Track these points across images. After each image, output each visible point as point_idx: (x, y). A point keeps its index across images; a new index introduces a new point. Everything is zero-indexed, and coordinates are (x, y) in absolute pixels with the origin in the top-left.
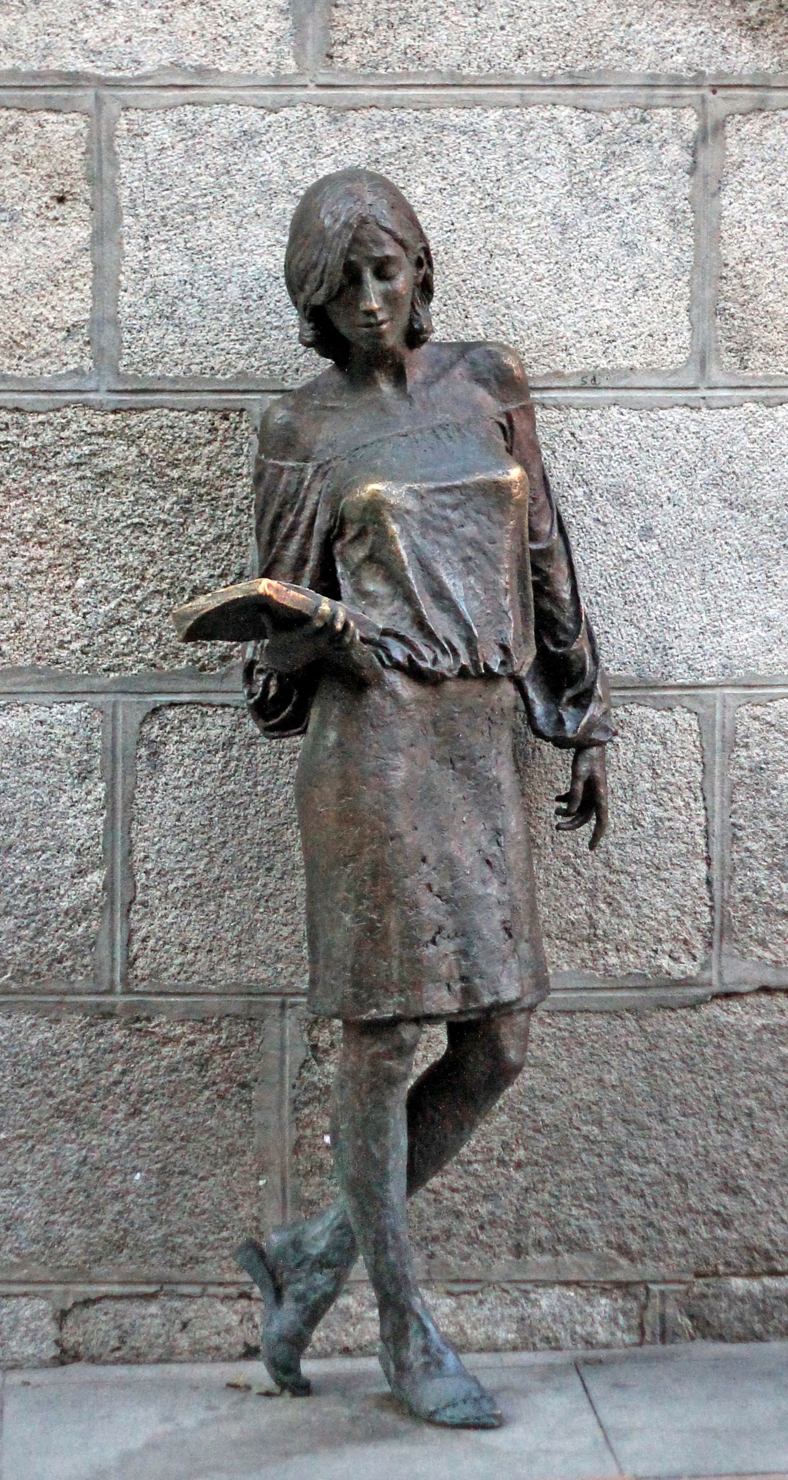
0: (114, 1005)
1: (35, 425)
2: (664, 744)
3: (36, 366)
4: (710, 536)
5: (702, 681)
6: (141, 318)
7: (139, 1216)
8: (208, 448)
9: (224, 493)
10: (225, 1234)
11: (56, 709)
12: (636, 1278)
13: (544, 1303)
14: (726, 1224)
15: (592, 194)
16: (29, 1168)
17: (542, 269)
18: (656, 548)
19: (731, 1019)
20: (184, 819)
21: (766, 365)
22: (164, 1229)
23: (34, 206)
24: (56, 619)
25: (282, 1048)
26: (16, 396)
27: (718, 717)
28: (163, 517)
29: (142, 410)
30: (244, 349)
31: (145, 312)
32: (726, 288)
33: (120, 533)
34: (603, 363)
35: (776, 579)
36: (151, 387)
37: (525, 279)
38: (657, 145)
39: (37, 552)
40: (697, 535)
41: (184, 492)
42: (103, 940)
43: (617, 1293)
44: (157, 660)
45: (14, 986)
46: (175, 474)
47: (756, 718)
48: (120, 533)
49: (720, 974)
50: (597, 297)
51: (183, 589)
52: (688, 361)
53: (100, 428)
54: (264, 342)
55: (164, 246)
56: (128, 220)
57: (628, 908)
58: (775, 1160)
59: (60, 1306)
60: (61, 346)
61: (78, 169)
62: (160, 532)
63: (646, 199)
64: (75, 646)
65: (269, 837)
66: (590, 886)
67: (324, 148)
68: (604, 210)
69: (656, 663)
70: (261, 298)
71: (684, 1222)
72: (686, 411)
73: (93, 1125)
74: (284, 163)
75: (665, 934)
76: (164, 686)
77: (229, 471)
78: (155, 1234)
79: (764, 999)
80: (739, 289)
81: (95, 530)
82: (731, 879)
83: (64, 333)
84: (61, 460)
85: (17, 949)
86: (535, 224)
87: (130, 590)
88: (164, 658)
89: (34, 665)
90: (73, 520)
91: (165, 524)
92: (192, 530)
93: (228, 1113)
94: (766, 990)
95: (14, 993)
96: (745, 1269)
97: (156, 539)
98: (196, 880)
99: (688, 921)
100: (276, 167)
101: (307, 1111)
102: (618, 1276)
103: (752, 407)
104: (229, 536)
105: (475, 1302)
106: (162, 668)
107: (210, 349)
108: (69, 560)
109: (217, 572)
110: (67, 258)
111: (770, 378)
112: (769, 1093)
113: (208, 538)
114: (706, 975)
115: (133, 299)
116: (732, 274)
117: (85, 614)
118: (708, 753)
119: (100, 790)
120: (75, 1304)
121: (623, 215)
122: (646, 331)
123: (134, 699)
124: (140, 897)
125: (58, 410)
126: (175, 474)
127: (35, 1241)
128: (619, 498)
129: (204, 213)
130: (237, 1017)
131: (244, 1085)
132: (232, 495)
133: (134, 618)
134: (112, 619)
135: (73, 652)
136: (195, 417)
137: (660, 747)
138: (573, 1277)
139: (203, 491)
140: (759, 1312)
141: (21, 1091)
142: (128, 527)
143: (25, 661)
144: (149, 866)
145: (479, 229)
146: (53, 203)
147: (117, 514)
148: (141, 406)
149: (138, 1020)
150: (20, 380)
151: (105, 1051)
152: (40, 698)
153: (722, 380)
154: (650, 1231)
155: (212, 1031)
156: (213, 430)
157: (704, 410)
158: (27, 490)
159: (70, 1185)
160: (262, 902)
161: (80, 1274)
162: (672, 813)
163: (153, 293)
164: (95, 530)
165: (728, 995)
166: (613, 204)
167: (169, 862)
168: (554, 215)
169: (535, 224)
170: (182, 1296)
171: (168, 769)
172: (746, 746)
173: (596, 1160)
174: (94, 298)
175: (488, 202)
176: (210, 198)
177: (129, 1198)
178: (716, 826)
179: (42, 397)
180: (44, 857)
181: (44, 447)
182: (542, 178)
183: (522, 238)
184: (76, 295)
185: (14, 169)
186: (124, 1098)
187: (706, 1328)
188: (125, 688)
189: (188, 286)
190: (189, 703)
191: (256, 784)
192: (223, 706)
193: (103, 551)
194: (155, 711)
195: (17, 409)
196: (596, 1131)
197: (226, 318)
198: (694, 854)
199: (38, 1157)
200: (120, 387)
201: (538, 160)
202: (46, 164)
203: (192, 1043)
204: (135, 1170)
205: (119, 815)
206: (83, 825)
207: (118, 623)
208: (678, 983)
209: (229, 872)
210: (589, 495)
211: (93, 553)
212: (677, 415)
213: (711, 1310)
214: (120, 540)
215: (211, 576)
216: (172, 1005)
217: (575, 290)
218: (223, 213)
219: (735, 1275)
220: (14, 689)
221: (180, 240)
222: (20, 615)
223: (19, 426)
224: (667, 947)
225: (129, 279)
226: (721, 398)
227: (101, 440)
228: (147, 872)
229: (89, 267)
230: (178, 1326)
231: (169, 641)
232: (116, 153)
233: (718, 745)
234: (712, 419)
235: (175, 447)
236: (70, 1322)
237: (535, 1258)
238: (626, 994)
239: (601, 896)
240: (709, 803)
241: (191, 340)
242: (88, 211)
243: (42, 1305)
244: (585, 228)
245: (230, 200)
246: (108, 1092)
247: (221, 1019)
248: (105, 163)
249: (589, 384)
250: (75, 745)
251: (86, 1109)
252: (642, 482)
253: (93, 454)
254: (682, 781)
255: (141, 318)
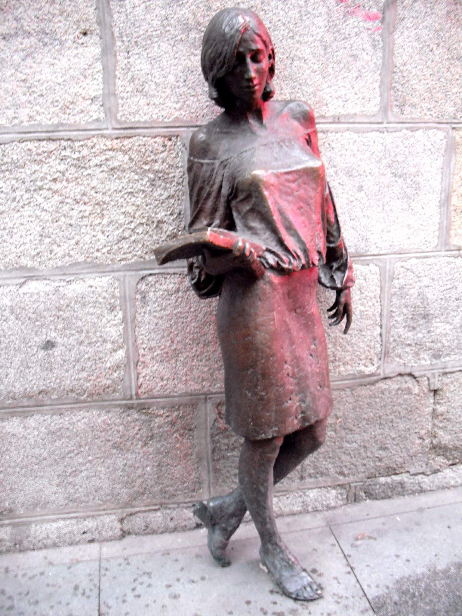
0: (133, 404)
1: (79, 147)
2: (365, 280)
3: (77, 118)
4: (386, 189)
5: (382, 252)
6: (127, 92)
7: (151, 483)
8: (161, 155)
9: (171, 176)
10: (185, 485)
11: (98, 279)
12: (346, 482)
13: (311, 495)
14: (380, 460)
15: (338, 31)
16: (103, 469)
17: (316, 67)
18: (364, 195)
19: (387, 387)
20: (159, 325)
21: (412, 112)
22: (161, 486)
23: (71, 37)
24: (95, 238)
25: (206, 415)
26: (68, 133)
27: (388, 267)
28: (142, 188)
29: (129, 138)
30: (178, 106)
31: (129, 89)
32: (395, 77)
33: (122, 197)
34: (343, 112)
35: (413, 208)
36: (133, 126)
37: (308, 72)
38: (367, 9)
39: (83, 208)
40: (381, 189)
41: (152, 176)
42: (127, 378)
43: (338, 488)
44: (143, 255)
45: (89, 399)
46: (147, 167)
47: (402, 267)
48: (122, 197)
49: (384, 371)
50: (340, 81)
51: (153, 222)
52: (379, 111)
53: (110, 147)
54: (187, 103)
55: (137, 56)
56: (119, 43)
57: (349, 348)
58: (400, 436)
59: (120, 517)
60: (89, 108)
61: (93, 18)
62: (141, 195)
63: (362, 34)
64: (105, 250)
65: (198, 330)
66: (334, 340)
67: (214, 7)
68: (343, 39)
69: (363, 245)
70: (185, 81)
71: (365, 462)
72: (378, 133)
73: (128, 450)
74: (194, 14)
75: (363, 357)
76: (147, 267)
77: (172, 165)
78: (157, 488)
79: (399, 378)
80: (401, 78)
81: (110, 196)
82: (389, 333)
83: (90, 101)
84: (92, 163)
85: (89, 385)
86: (313, 45)
87: (128, 223)
88: (146, 253)
89: (85, 260)
90: (100, 192)
91: (144, 191)
92: (155, 194)
93: (185, 441)
94: (400, 375)
95: (89, 402)
96: (386, 474)
97: (139, 199)
98: (166, 350)
99: (372, 351)
100: (191, 16)
101: (217, 437)
102: (340, 483)
103: (405, 131)
104: (173, 196)
105: (285, 498)
106: (145, 259)
107: (162, 107)
108: (99, 211)
109: (169, 213)
110: (89, 63)
111: (414, 119)
112: (399, 413)
113: (163, 197)
114: (378, 372)
115: (123, 83)
116: (398, 71)
117: (108, 236)
118: (383, 283)
119: (120, 315)
120: (127, 515)
121: (352, 42)
122: (361, 96)
123: (133, 273)
124: (141, 359)
125: (89, 139)
126: (147, 167)
127: (108, 495)
128: (349, 173)
129: (156, 39)
130: (186, 404)
131: (190, 430)
132: (174, 177)
133: (131, 236)
134: (121, 237)
135: (104, 253)
136: (155, 140)
137: (364, 281)
138: (322, 485)
139: (160, 175)
140: (390, 488)
141: (96, 441)
142: (126, 193)
143: (81, 259)
144: (144, 346)
145: (287, 48)
146: (81, 36)
147: (120, 188)
148: (129, 135)
149: (144, 409)
150: (70, 125)
151: (131, 422)
152: (90, 275)
153: (392, 119)
154: (352, 466)
155: (176, 410)
156: (164, 146)
157: (385, 132)
158: (76, 178)
159: (121, 474)
160: (196, 358)
161: (128, 504)
162: (367, 308)
163: (133, 79)
164: (110, 196)
165: (385, 378)
166: (348, 36)
167: (153, 344)
168: (321, 42)
169: (313, 45)
170: (170, 509)
171: (150, 303)
172: (398, 279)
173: (333, 444)
174: (104, 83)
175: (291, 34)
176: (159, 32)
177: (146, 476)
178: (385, 312)
179: (81, 133)
180: (97, 345)
181: (83, 157)
182: (315, 23)
183: (306, 52)
184: (95, 82)
185: (60, 18)
186: (140, 440)
187: (370, 495)
188: (129, 268)
189: (149, 76)
190: (158, 274)
191: (190, 308)
192: (174, 274)
193: (115, 205)
194: (143, 278)
195: (69, 139)
196: (333, 433)
197: (168, 91)
198: (377, 325)
199: (107, 465)
200: (119, 126)
201: (313, 14)
202: (76, 15)
203: (168, 416)
204: (147, 466)
205: (129, 325)
206: (114, 332)
207: (124, 238)
208: (369, 376)
209: (180, 346)
210: (336, 173)
211: (110, 207)
212: (374, 135)
213: (373, 490)
214: (122, 200)
215: (166, 215)
216: (159, 402)
217: (330, 77)
218: (166, 39)
219: (383, 476)
220: (78, 272)
221: (145, 53)
222: (77, 238)
223: (71, 148)
224: (363, 362)
225: (120, 73)
226: (393, 128)
227: (111, 153)
228: (144, 349)
229: (101, 67)
230: (169, 519)
231: (147, 246)
232: (111, 9)
233: (387, 279)
234: (388, 138)
235: (147, 154)
236: (125, 521)
237: (308, 480)
238: (346, 382)
239: (337, 344)
240: (382, 303)
241: (152, 103)
242: (98, 39)
243: (113, 517)
244: (335, 48)
245: (168, 33)
246: (134, 437)
247: (179, 406)
248: (106, 15)
249: (336, 121)
250: (107, 296)
251: (124, 445)
252: (358, 166)
253: (107, 160)
254: (372, 295)
255: (127, 92)
